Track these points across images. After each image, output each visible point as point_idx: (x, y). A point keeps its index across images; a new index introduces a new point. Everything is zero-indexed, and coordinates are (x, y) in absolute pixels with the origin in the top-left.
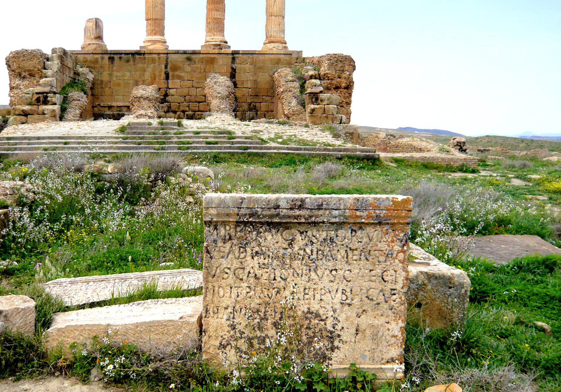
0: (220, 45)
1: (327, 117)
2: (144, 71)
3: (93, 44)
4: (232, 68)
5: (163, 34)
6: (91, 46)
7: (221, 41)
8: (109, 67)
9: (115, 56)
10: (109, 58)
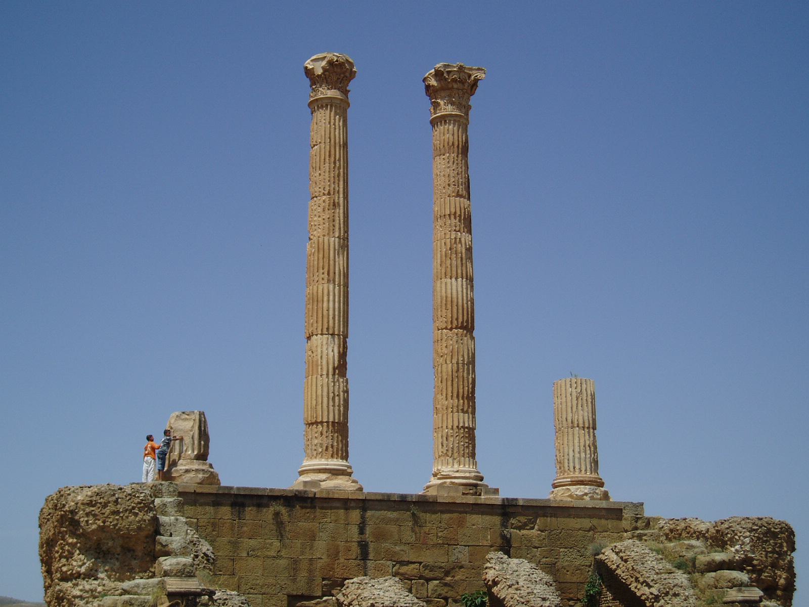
0: (476, 486)
2: (313, 538)
3: (197, 470)
4: (503, 537)
5: (345, 457)
6: (192, 475)
8: (232, 528)
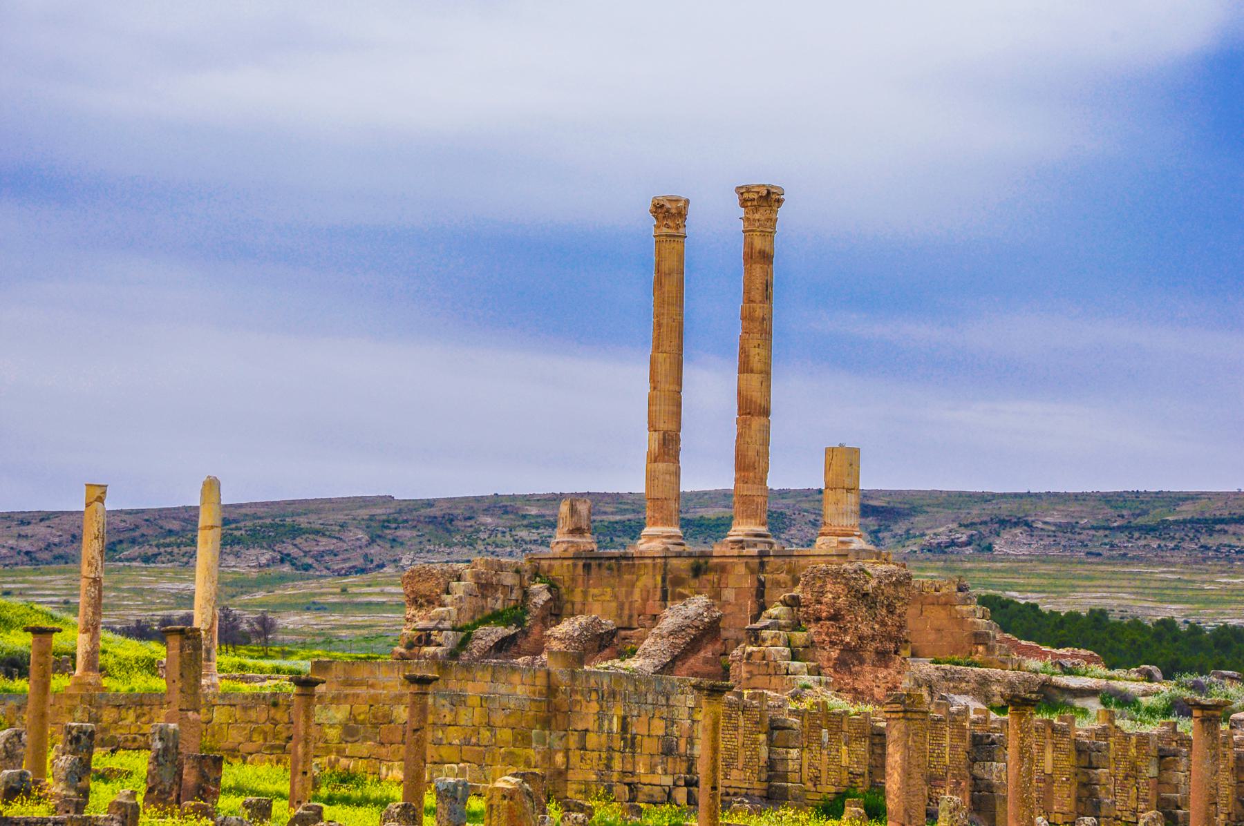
0: (741, 541)
1: (767, 665)
4: (759, 581)
7: (747, 535)
9: (593, 563)
10: (584, 565)
